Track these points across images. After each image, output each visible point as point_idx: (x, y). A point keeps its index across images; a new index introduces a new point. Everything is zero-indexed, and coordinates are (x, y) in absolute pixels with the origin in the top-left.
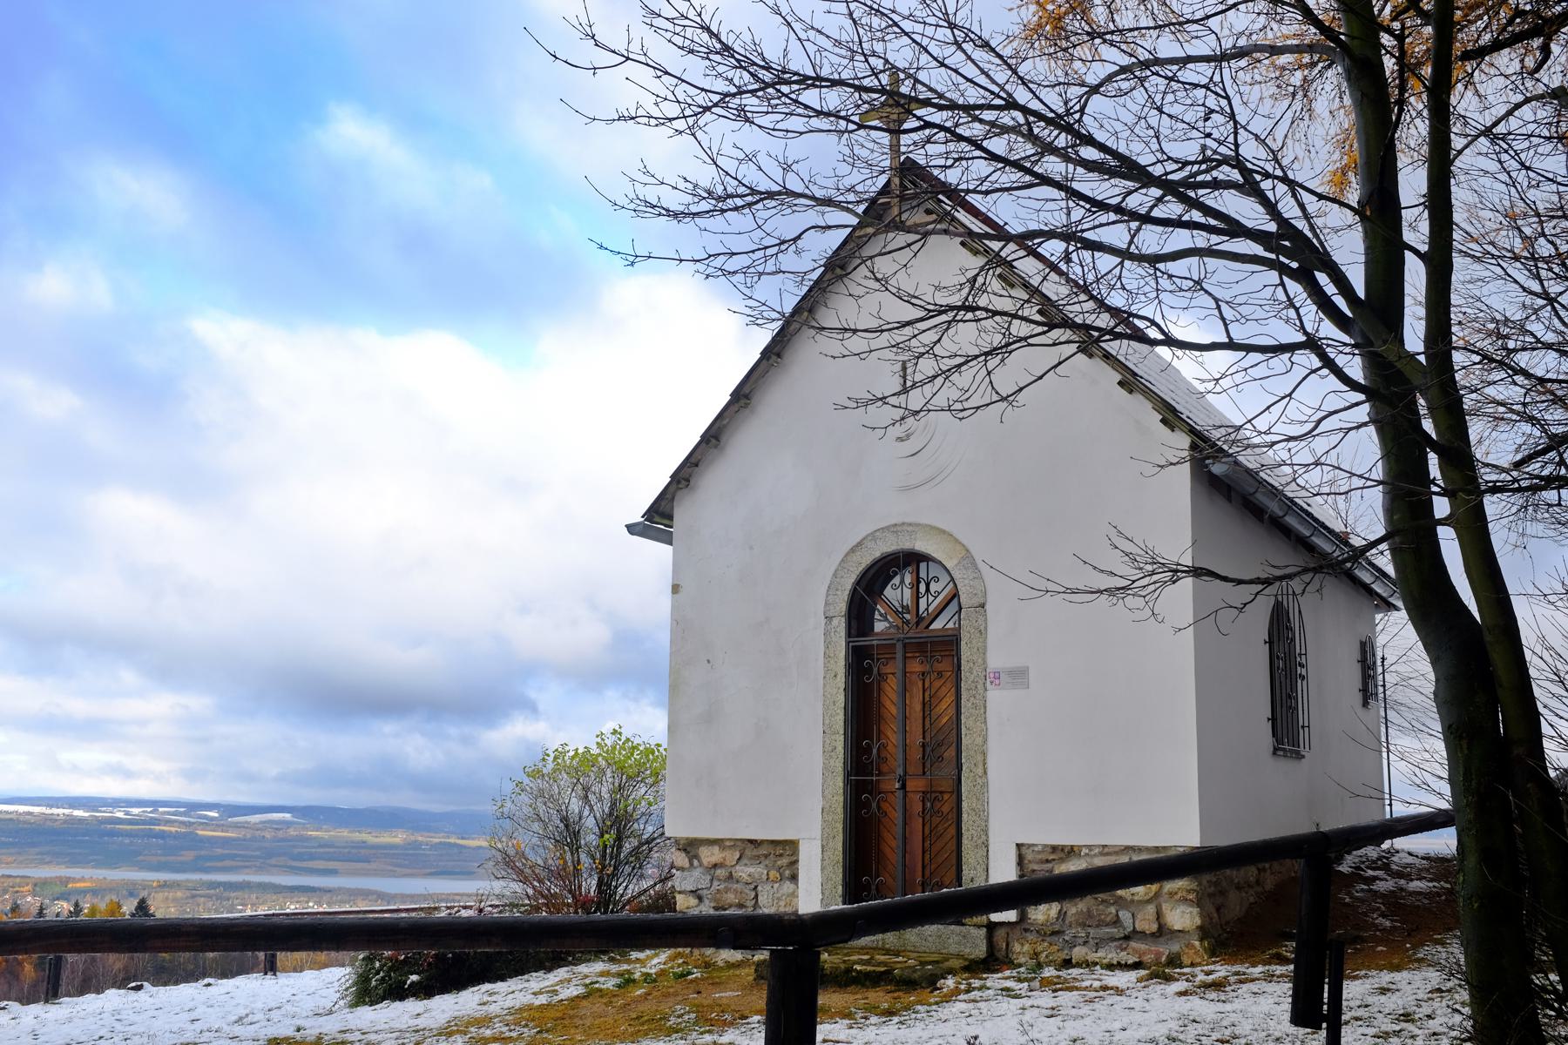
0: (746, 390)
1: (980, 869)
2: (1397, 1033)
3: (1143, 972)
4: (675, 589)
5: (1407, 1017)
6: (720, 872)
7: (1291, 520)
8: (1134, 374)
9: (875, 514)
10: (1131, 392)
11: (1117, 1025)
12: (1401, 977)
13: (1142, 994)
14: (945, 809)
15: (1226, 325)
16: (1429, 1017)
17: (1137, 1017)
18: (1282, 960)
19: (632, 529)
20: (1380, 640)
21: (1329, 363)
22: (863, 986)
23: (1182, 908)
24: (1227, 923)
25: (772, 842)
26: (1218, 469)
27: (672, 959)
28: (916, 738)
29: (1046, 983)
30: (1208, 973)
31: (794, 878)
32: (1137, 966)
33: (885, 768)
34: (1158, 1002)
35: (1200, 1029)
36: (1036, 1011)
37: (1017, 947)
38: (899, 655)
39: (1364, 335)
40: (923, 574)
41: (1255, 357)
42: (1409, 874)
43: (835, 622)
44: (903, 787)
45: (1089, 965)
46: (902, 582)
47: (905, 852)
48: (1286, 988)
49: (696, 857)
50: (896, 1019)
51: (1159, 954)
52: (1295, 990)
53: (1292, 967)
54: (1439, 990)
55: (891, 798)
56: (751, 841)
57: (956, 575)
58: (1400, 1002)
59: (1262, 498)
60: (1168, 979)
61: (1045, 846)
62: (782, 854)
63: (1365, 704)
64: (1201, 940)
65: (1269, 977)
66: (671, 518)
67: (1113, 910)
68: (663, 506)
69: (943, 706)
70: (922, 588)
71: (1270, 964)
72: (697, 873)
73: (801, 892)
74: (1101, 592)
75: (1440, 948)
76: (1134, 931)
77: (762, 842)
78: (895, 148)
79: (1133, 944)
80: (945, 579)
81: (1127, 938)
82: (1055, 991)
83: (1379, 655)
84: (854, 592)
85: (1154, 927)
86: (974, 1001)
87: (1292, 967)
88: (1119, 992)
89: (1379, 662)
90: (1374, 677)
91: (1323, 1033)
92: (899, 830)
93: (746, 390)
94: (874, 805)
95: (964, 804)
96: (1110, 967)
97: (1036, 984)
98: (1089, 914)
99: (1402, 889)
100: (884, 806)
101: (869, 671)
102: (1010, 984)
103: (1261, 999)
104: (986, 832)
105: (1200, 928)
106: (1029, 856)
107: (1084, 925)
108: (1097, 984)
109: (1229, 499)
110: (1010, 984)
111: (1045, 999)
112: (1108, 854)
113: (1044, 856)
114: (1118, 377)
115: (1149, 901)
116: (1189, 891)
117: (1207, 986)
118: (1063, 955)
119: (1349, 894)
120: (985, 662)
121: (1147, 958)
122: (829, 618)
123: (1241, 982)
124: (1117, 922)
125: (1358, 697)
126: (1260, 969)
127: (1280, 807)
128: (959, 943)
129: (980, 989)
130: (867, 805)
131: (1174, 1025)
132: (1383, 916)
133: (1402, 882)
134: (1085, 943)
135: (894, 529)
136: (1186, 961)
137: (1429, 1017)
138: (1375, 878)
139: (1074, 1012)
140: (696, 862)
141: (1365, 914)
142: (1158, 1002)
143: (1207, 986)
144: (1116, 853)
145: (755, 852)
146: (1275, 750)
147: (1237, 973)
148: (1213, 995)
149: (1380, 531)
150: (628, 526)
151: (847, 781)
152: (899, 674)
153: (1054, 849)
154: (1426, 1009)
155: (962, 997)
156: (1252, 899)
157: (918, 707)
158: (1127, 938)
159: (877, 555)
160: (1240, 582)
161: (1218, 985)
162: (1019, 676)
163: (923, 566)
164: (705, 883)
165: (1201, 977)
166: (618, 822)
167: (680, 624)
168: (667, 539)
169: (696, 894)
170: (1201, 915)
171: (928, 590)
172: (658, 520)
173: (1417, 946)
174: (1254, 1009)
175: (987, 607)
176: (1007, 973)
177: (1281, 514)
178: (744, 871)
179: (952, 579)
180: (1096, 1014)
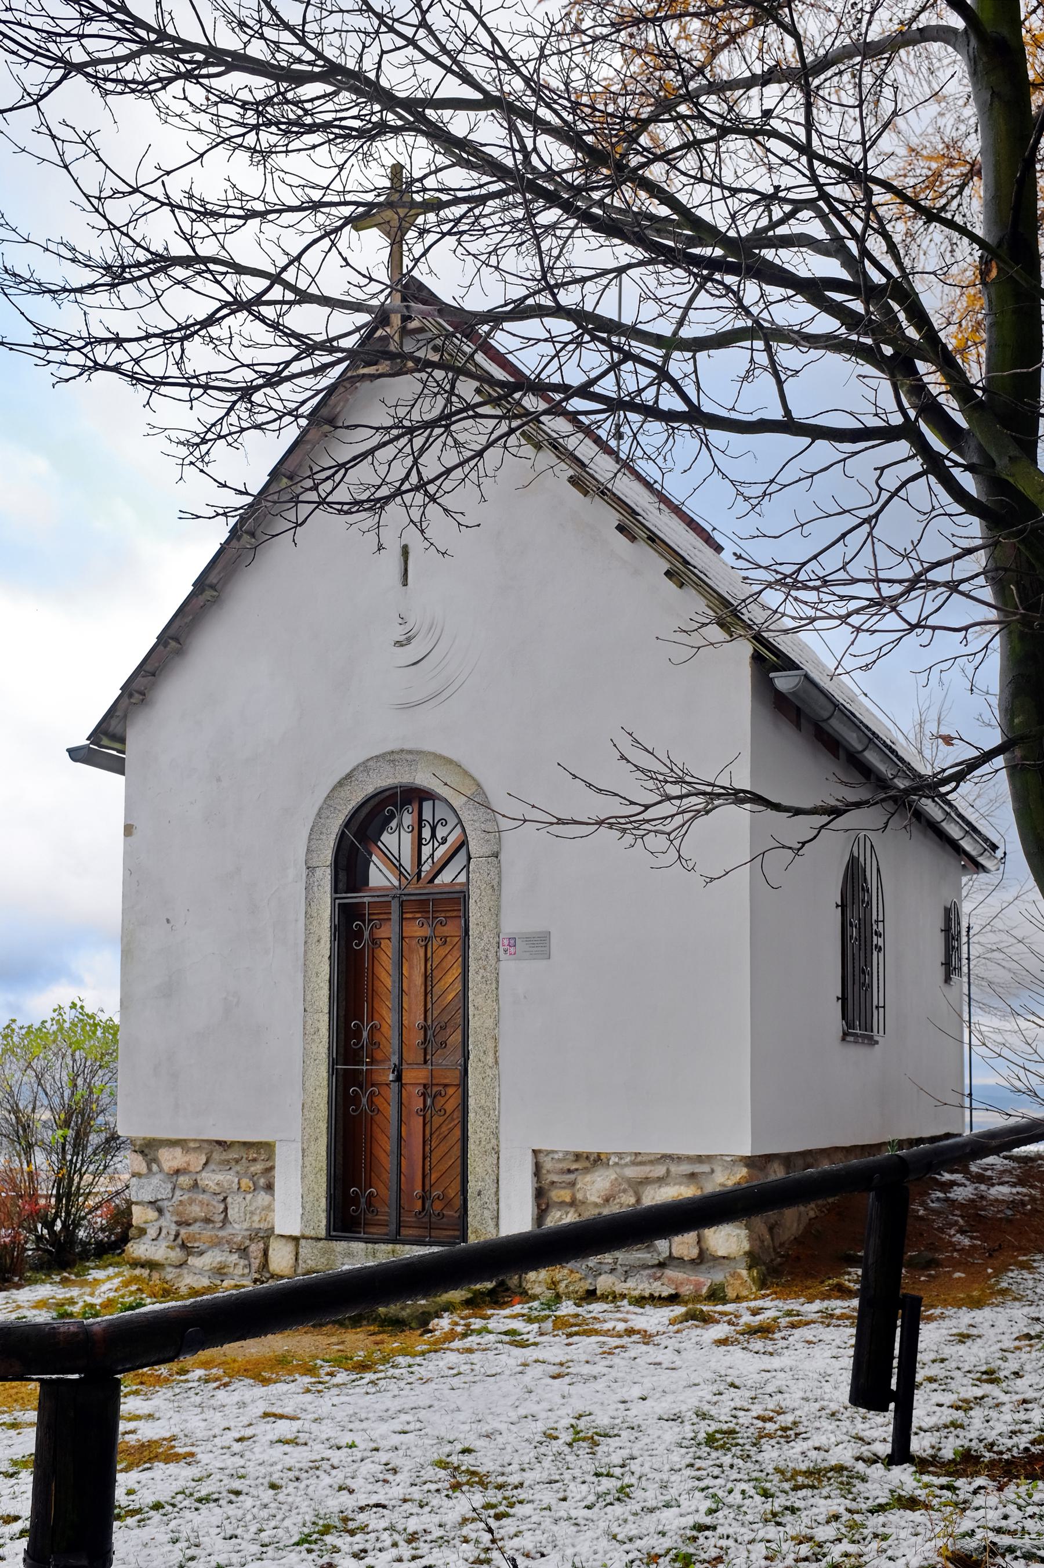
0: (213, 579)
1: (490, 1180)
2: (979, 1400)
3: (680, 1310)
4: (128, 830)
5: (990, 1376)
6: (184, 1180)
7: (871, 757)
8: (686, 562)
9: (364, 736)
10: (681, 585)
11: (636, 1392)
12: (983, 1316)
13: (673, 1343)
14: (450, 1107)
15: (780, 383)
16: (1017, 1374)
17: (664, 1378)
18: (843, 1292)
19: (76, 754)
20: (966, 907)
21: (935, 465)
24: (782, 1245)
25: (245, 1144)
26: (784, 682)
27: (126, 1284)
28: (415, 1017)
29: (560, 1324)
30: (755, 1312)
31: (270, 1187)
32: (673, 1299)
33: (379, 1055)
34: (691, 1355)
35: (739, 1398)
36: (541, 1367)
38: (395, 916)
39: (981, 450)
40: (427, 815)
41: (825, 450)
42: (990, 1178)
43: (319, 873)
44: (399, 1078)
45: (614, 1297)
46: (400, 825)
47: (400, 1155)
48: (847, 1334)
49: (155, 1160)
50: (369, 1376)
51: (699, 1285)
52: (859, 1336)
53: (855, 1303)
54: (1028, 1337)
55: (384, 1090)
56: (219, 1143)
57: (465, 816)
58: (982, 1355)
59: (836, 725)
60: (706, 1319)
61: (567, 1153)
62: (255, 1157)
63: (947, 980)
64: (750, 1268)
65: (828, 1318)
66: (122, 740)
68: (114, 726)
69: (449, 978)
70: (426, 833)
71: (828, 1297)
72: (156, 1180)
73: (277, 1205)
74: (600, 823)
75: (1027, 1276)
76: (671, 1257)
77: (233, 1143)
78: (395, 259)
79: (669, 1273)
80: (452, 821)
81: (661, 1265)
82: (570, 1335)
83: (964, 925)
84: (342, 837)
85: (694, 1253)
86: (470, 1351)
87: (855, 1303)
88: (647, 1338)
89: (964, 933)
90: (958, 949)
91: (890, 1415)
93: (213, 579)
94: (364, 1100)
95: (471, 1101)
96: (641, 1301)
97: (548, 1325)
99: (982, 1197)
100: (379, 1101)
101: (359, 935)
102: (518, 1325)
103: (816, 1350)
105: (749, 1254)
106: (548, 1164)
108: (621, 1326)
109: (798, 726)
110: (518, 1325)
111: (554, 1349)
112: (642, 1163)
113: (565, 1166)
114: (666, 566)
117: (753, 1331)
118: (587, 1285)
119: (923, 1204)
120: (497, 925)
121: (686, 1290)
122: (311, 869)
123: (793, 1326)
125: (940, 972)
126: (817, 1305)
127: (852, 1109)
129: (479, 1332)
130: (356, 1099)
131: (706, 1392)
132: (962, 1232)
133: (983, 1187)
134: (612, 1271)
135: (391, 757)
136: (731, 1294)
137: (1017, 1374)
138: (953, 1184)
139: (586, 1370)
140: (155, 1167)
141: (941, 1230)
142: (691, 1355)
143: (753, 1331)
144: (651, 1162)
145: (225, 1156)
146: (845, 1034)
147: (789, 1313)
148: (758, 1345)
149: (994, 738)
150: (70, 751)
151: (332, 1071)
152: (395, 939)
153: (578, 1156)
154: (1013, 1365)
155: (457, 1344)
156: (812, 1214)
157: (419, 980)
158: (661, 1265)
159: (370, 790)
160: (797, 812)
161: (764, 1331)
162: (539, 944)
163: (427, 806)
164: (165, 1192)
165: (747, 1318)
166: (79, 1119)
167: (136, 877)
168: (117, 766)
169: (155, 1204)
170: (751, 1239)
171: (433, 835)
172: (105, 746)
173: (1002, 1270)
174: (807, 1365)
175: (503, 856)
176: (517, 1309)
177: (860, 748)
178: (211, 1179)
179: (460, 822)
180: (614, 1373)
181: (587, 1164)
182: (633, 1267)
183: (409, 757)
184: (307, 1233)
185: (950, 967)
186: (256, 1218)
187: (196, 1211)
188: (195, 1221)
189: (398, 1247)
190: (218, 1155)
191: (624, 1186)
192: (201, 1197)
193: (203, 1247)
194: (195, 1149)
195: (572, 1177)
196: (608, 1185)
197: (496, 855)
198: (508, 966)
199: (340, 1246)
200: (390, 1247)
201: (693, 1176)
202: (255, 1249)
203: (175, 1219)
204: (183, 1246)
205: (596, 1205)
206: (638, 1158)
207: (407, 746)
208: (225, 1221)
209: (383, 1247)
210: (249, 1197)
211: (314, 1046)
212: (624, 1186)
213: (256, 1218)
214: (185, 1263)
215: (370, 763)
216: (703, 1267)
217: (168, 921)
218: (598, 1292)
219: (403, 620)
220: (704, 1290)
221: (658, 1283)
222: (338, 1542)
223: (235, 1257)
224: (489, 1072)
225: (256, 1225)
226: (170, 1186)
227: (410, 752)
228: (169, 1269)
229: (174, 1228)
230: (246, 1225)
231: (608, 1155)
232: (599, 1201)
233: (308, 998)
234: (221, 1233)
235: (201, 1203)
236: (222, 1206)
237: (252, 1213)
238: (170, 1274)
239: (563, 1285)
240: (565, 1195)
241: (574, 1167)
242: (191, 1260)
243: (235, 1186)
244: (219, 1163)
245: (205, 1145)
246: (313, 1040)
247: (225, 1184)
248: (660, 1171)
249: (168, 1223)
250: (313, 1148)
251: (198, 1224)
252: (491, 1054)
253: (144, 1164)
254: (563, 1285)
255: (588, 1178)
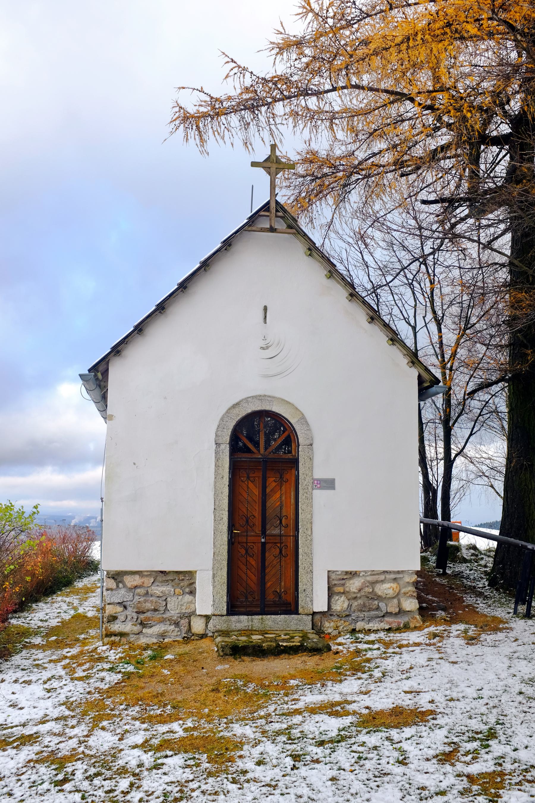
22: (289, 654)
23: (411, 600)
25: (177, 572)
31: (192, 593)
37: (327, 624)
43: (223, 446)
51: (399, 623)
61: (342, 572)
62: (185, 580)
67: (376, 602)
72: (123, 591)
76: (387, 613)
77: (170, 572)
79: (386, 619)
85: (397, 610)
92: (377, 577)
95: (300, 551)
98: (364, 605)
104: (311, 564)
106: (333, 576)
107: (361, 611)
112: (374, 575)
115: (394, 598)
116: (414, 592)
118: (352, 627)
124: (378, 608)
128: (297, 624)
135: (260, 398)
140: (121, 585)
144: (378, 574)
145: (164, 578)
153: (347, 573)
158: (383, 616)
159: (249, 411)
162: (329, 484)
175: (314, 446)
178: (158, 590)
181: (350, 576)
182: (372, 618)
183: (269, 399)
184: (216, 613)
185: (265, 309)
186: (184, 607)
187: (148, 606)
188: (148, 611)
189: (264, 616)
190: (160, 578)
191: (368, 584)
192: (151, 599)
193: (153, 623)
194: (147, 576)
195: (344, 581)
196: (360, 584)
197: (311, 445)
198: (317, 493)
199: (234, 618)
200: (260, 617)
201: (395, 579)
202: (184, 622)
203: (135, 610)
204: (141, 623)
205: (354, 593)
206: (373, 573)
207: (266, 394)
208: (166, 610)
209: (257, 617)
210: (180, 597)
211: (220, 526)
212: (368, 584)
213: (184, 607)
214: (141, 632)
215: (249, 399)
216: (399, 616)
217: (134, 464)
218: (357, 629)
219: (265, 339)
220: (402, 625)
221: (382, 624)
222: (137, 714)
223: (172, 627)
224: (309, 538)
225: (184, 611)
226: (132, 594)
227: (269, 396)
228: (132, 636)
229: (135, 615)
230: (177, 611)
231: (360, 572)
232: (356, 591)
233: (217, 503)
234: (164, 616)
235: (152, 602)
236: (164, 603)
237: (182, 605)
238: (132, 638)
239: (341, 627)
240: (341, 589)
241: (345, 577)
242: (144, 631)
243: (172, 593)
244: (162, 582)
245: (154, 573)
246: (220, 523)
247: (167, 592)
248: (382, 577)
249: (130, 612)
250: (219, 573)
251: (150, 612)
252: (310, 530)
253: (115, 584)
254: (341, 627)
255: (351, 582)
